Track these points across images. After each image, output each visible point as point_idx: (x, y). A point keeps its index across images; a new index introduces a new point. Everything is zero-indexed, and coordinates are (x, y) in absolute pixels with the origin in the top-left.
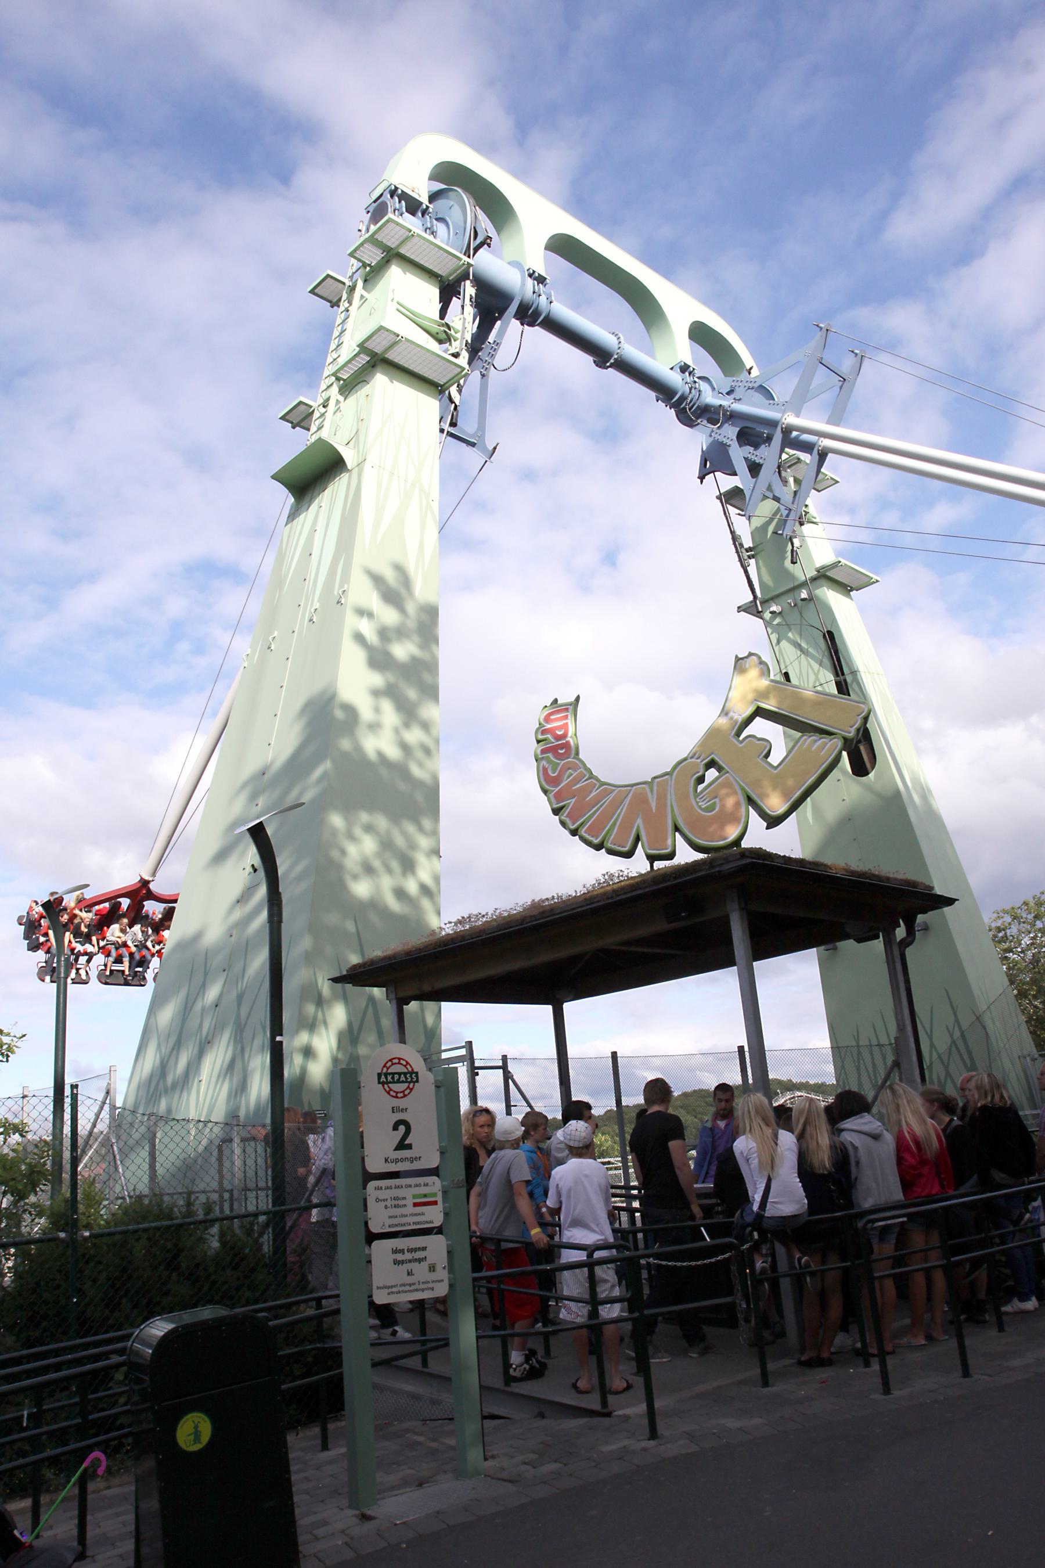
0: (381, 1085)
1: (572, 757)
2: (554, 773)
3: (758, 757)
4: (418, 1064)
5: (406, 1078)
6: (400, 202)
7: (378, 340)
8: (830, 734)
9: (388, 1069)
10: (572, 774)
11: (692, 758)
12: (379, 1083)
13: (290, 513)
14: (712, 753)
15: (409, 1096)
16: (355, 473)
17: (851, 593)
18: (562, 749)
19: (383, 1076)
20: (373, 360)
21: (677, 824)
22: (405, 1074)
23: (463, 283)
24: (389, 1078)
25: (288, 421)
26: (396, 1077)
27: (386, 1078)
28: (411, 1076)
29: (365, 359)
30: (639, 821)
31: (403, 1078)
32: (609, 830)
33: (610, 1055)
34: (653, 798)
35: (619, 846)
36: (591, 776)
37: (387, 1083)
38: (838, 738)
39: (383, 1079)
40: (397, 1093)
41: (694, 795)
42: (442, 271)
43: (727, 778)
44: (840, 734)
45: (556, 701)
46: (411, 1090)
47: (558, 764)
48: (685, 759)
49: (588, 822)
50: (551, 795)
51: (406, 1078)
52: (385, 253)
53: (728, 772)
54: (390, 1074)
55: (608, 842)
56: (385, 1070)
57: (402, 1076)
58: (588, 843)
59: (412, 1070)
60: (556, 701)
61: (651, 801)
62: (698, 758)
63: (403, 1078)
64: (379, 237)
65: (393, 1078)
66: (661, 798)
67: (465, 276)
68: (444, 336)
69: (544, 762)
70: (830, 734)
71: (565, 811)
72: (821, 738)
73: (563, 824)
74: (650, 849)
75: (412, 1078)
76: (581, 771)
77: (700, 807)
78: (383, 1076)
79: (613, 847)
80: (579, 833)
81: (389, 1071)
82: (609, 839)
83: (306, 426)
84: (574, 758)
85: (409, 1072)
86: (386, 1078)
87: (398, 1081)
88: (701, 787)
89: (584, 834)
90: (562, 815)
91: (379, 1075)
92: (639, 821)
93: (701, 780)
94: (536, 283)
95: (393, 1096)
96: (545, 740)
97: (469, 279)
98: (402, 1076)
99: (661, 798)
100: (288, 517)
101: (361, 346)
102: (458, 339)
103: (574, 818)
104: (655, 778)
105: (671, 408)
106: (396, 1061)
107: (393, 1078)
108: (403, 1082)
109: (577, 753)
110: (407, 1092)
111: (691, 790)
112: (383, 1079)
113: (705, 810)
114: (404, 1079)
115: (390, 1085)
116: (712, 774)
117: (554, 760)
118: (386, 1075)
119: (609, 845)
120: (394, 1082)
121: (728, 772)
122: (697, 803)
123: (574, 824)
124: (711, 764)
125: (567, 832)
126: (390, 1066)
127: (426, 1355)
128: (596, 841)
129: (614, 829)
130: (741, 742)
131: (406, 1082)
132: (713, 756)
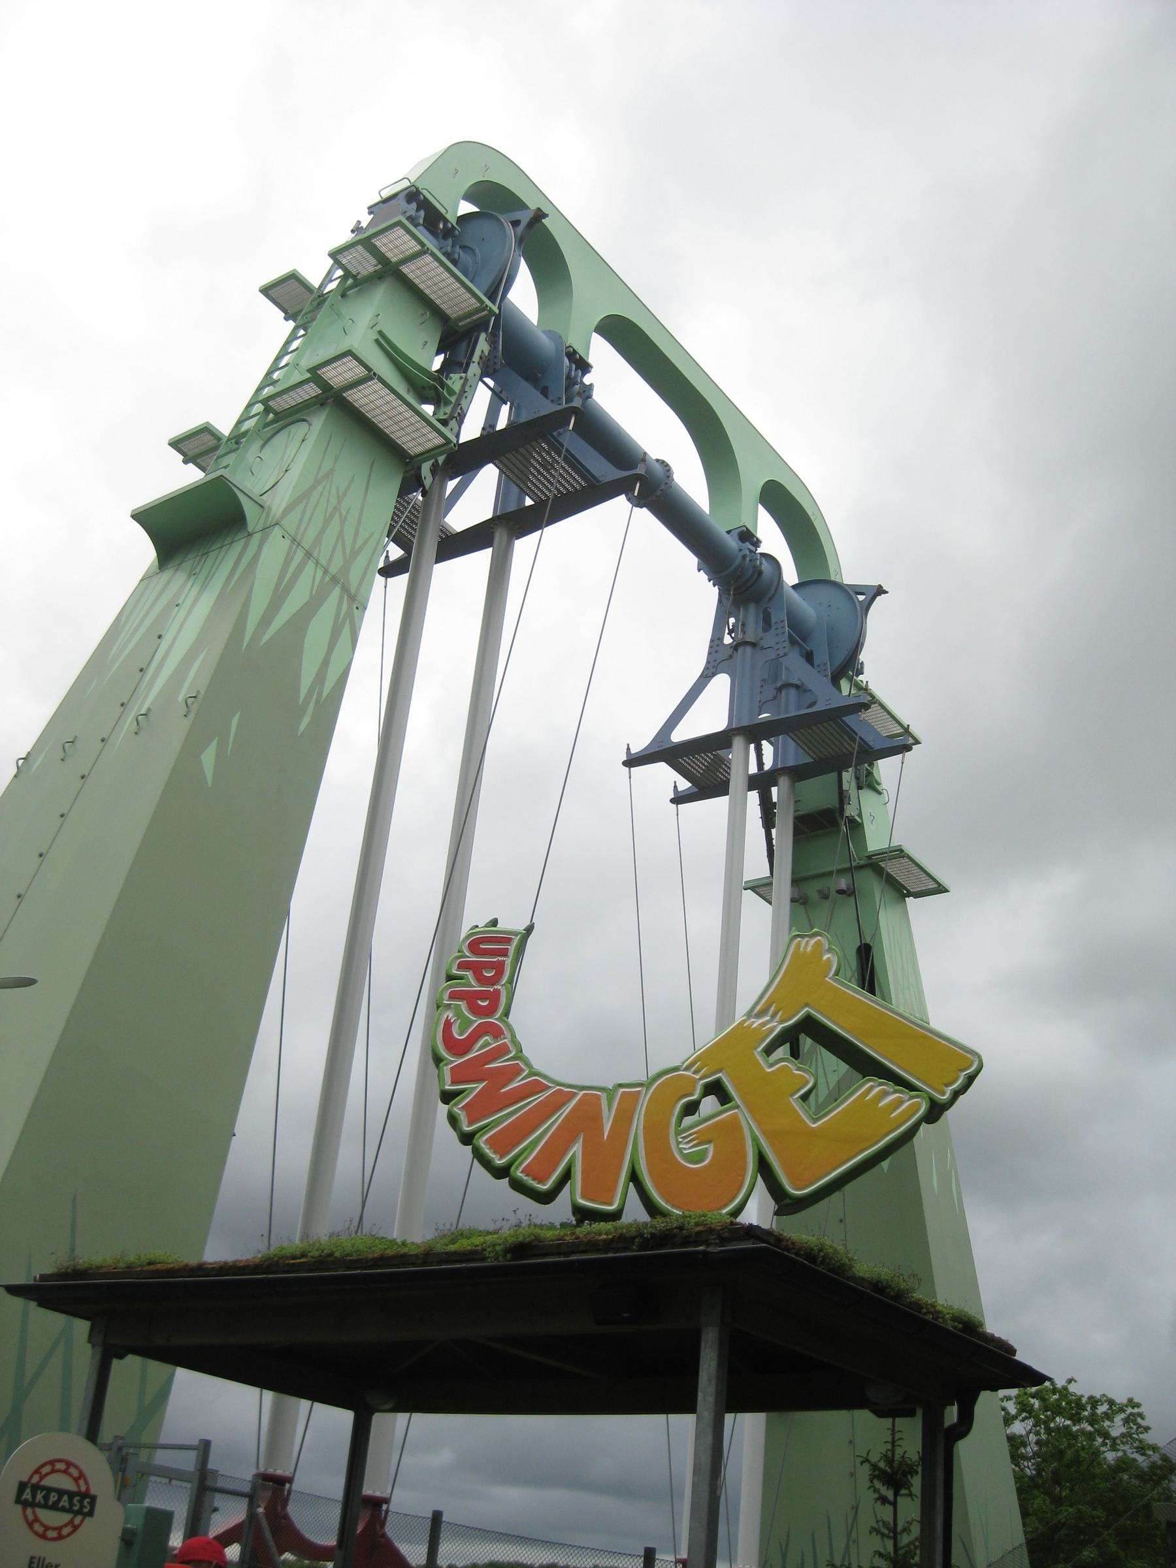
0: (19, 1508)
1: (831, 976)
2: (461, 1034)
3: (792, 1095)
4: (101, 1481)
5: (71, 1504)
6: (417, 210)
7: (340, 370)
8: (911, 1087)
9: (42, 1478)
10: (489, 1044)
11: (688, 1068)
12: (18, 1500)
13: (144, 576)
14: (720, 1071)
15: (68, 1539)
16: (256, 538)
17: (907, 899)
18: (483, 999)
19: (28, 1491)
20: (324, 396)
21: (637, 1167)
22: (71, 1495)
23: (476, 334)
24: (40, 1496)
25: (179, 451)
26: (53, 1497)
27: (34, 1496)
28: (81, 1502)
29: (312, 390)
30: (577, 1148)
31: (64, 1502)
32: (525, 1149)
33: (430, 1515)
34: (609, 1119)
35: (534, 1179)
36: (520, 1055)
37: (33, 1504)
38: (923, 1098)
39: (27, 1495)
40: (47, 1528)
41: (676, 1128)
42: (452, 312)
43: (735, 1117)
44: (927, 1092)
45: (494, 923)
46: (76, 1528)
47: (472, 1022)
48: (676, 1069)
49: (493, 1128)
50: (447, 1070)
51: (71, 1504)
52: (380, 266)
53: (737, 1107)
54: (43, 1488)
55: (517, 1168)
56: (35, 1479)
57: (65, 1497)
58: (486, 1163)
59: (88, 1489)
60: (494, 923)
61: (605, 1121)
62: (695, 1072)
63: (64, 1502)
64: (377, 242)
65: (46, 1497)
66: (624, 1118)
67: (481, 325)
68: (432, 393)
69: (450, 1014)
70: (911, 1087)
71: (460, 1102)
72: (896, 1092)
73: (453, 1120)
74: (584, 1196)
75: (82, 1507)
76: (505, 1043)
77: (680, 1150)
78: (28, 1491)
79: (525, 1178)
80: (474, 1141)
81: (45, 1482)
82: (520, 1164)
83: (203, 464)
84: (500, 1019)
85: (78, 1493)
86: (34, 1496)
87: (55, 1507)
88: (688, 1121)
89: (483, 1146)
90: (455, 1105)
91: (22, 1486)
92: (577, 1148)
93: (691, 1108)
94: (574, 366)
95: (36, 1533)
96: (460, 978)
97: (486, 330)
98: (65, 1497)
99: (624, 1118)
100: (141, 580)
101: (313, 370)
102: (451, 403)
103: (475, 1112)
104: (621, 1086)
105: (714, 586)
106: (37, 1527)
107: (46, 1497)
108: (63, 1509)
109: (507, 1014)
110: (65, 1531)
111: (674, 1120)
112: (27, 1495)
113: (689, 1158)
114: (67, 1504)
115: (38, 1511)
116: (709, 1104)
117: (467, 1015)
118: (36, 1488)
119: (519, 1174)
120: (45, 1506)
121: (737, 1107)
122: (679, 1143)
123: (470, 1124)
124: (716, 1089)
125: (453, 1136)
126: (47, 1474)
127: (371, 379)
128: (499, 1162)
129: (532, 1150)
130: (771, 1066)
131: (69, 1511)
132: (720, 1075)
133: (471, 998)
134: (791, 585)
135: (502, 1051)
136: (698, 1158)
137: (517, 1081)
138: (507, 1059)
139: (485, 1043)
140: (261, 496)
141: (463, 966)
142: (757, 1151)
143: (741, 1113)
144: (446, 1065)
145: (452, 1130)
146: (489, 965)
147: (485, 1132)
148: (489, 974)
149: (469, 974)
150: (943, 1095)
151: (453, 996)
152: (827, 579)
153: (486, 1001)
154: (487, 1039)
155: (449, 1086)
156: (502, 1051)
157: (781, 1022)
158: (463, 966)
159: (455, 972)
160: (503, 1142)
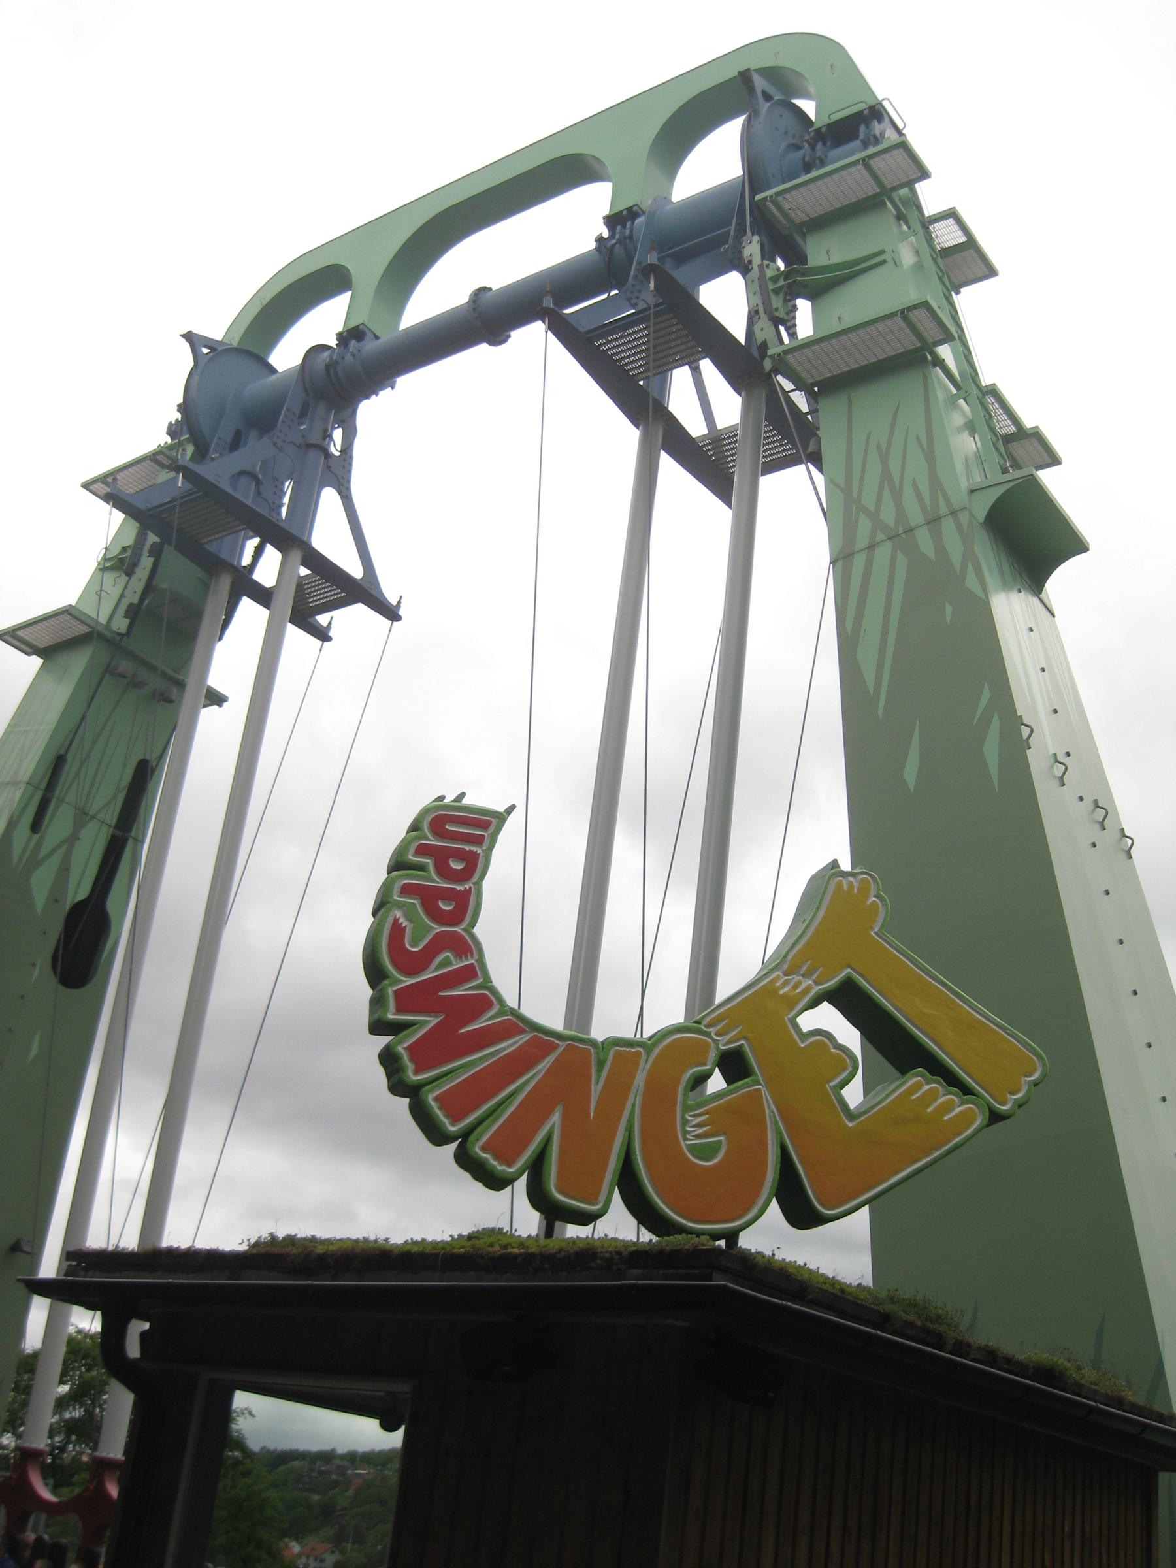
8: (966, 1090)
70: (966, 1090)
84: (464, 930)
89: (433, 1103)
92: (556, 1118)
99: (617, 1089)
103: (424, 1054)
109: (473, 924)
133: (429, 898)
134: (268, 612)
135: (468, 973)
136: (706, 1152)
137: (480, 1021)
138: (470, 987)
139: (447, 962)
140: (869, 434)
141: (422, 850)
142: (779, 1142)
143: (759, 1085)
144: (391, 985)
145: (821, 474)
146: (460, 855)
147: (437, 1086)
148: (457, 866)
149: (428, 861)
150: (1003, 1104)
151: (407, 890)
152: (263, 356)
153: (451, 905)
154: (448, 956)
155: (394, 1014)
156: (468, 973)
157: (817, 983)
158: (422, 850)
159: (411, 857)
160: (456, 1104)
